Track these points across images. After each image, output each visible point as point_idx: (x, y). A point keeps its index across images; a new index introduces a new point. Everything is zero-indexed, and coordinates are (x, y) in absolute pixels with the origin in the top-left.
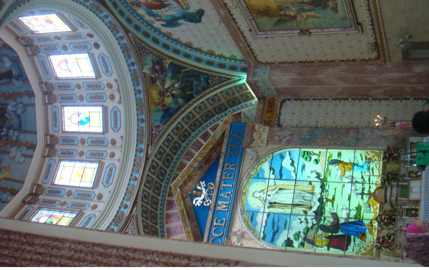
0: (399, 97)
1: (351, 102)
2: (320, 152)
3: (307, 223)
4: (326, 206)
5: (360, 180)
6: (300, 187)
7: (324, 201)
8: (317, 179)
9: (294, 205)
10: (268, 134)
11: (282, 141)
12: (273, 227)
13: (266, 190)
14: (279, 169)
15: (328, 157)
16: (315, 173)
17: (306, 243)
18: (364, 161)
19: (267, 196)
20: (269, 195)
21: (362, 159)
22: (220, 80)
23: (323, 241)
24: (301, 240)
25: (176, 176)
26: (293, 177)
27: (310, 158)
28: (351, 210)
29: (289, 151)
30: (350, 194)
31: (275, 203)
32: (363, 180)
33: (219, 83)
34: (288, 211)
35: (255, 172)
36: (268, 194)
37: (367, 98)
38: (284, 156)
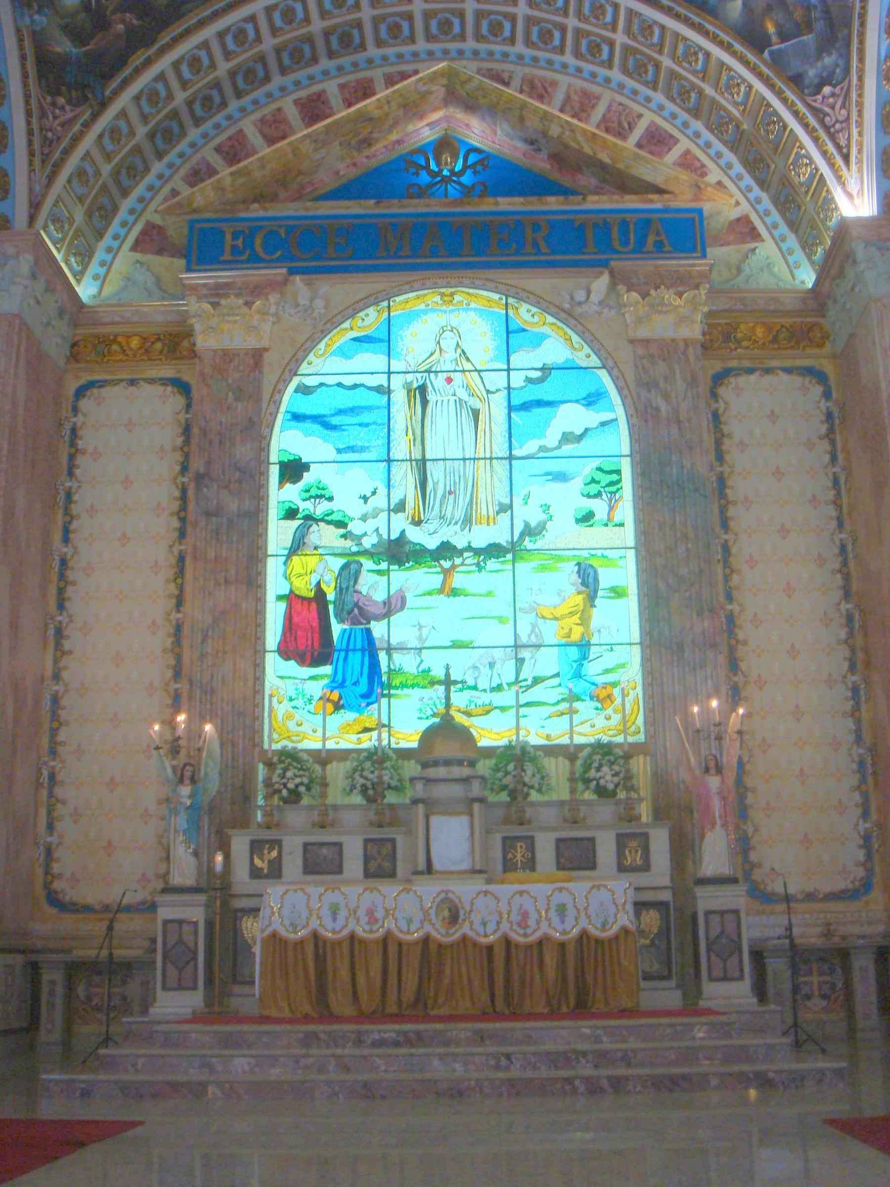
0: (870, 779)
1: (839, 610)
2: (622, 525)
3: (364, 518)
4: (426, 570)
5: (527, 673)
6: (488, 475)
7: (442, 562)
8: (519, 528)
9: (421, 464)
10: (673, 340)
11: (649, 391)
12: (340, 412)
13: (467, 366)
14: (546, 398)
15: (606, 553)
16: (543, 517)
17: (296, 524)
18: (600, 680)
19: (445, 375)
20: (449, 380)
21: (607, 671)
22: (838, 126)
23: (307, 578)
24: (306, 507)
25: (506, 76)
26: (521, 447)
27: (598, 495)
28: (420, 655)
29: (616, 419)
30: (476, 645)
31: (425, 403)
32: (529, 682)
33: (827, 128)
34: (401, 449)
35: (530, 319)
36: (452, 375)
37: (859, 666)
38: (596, 407)
